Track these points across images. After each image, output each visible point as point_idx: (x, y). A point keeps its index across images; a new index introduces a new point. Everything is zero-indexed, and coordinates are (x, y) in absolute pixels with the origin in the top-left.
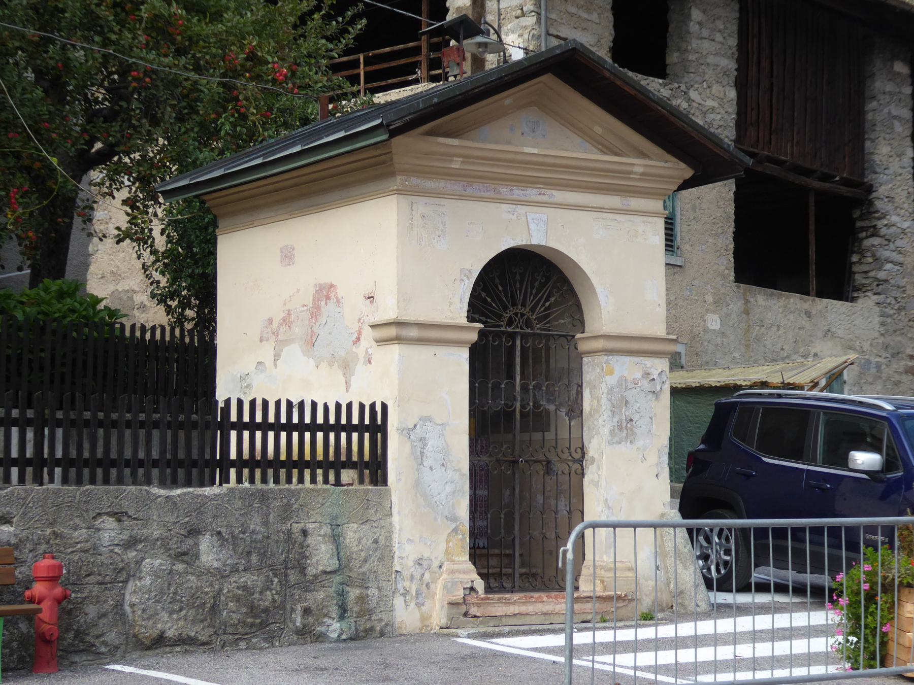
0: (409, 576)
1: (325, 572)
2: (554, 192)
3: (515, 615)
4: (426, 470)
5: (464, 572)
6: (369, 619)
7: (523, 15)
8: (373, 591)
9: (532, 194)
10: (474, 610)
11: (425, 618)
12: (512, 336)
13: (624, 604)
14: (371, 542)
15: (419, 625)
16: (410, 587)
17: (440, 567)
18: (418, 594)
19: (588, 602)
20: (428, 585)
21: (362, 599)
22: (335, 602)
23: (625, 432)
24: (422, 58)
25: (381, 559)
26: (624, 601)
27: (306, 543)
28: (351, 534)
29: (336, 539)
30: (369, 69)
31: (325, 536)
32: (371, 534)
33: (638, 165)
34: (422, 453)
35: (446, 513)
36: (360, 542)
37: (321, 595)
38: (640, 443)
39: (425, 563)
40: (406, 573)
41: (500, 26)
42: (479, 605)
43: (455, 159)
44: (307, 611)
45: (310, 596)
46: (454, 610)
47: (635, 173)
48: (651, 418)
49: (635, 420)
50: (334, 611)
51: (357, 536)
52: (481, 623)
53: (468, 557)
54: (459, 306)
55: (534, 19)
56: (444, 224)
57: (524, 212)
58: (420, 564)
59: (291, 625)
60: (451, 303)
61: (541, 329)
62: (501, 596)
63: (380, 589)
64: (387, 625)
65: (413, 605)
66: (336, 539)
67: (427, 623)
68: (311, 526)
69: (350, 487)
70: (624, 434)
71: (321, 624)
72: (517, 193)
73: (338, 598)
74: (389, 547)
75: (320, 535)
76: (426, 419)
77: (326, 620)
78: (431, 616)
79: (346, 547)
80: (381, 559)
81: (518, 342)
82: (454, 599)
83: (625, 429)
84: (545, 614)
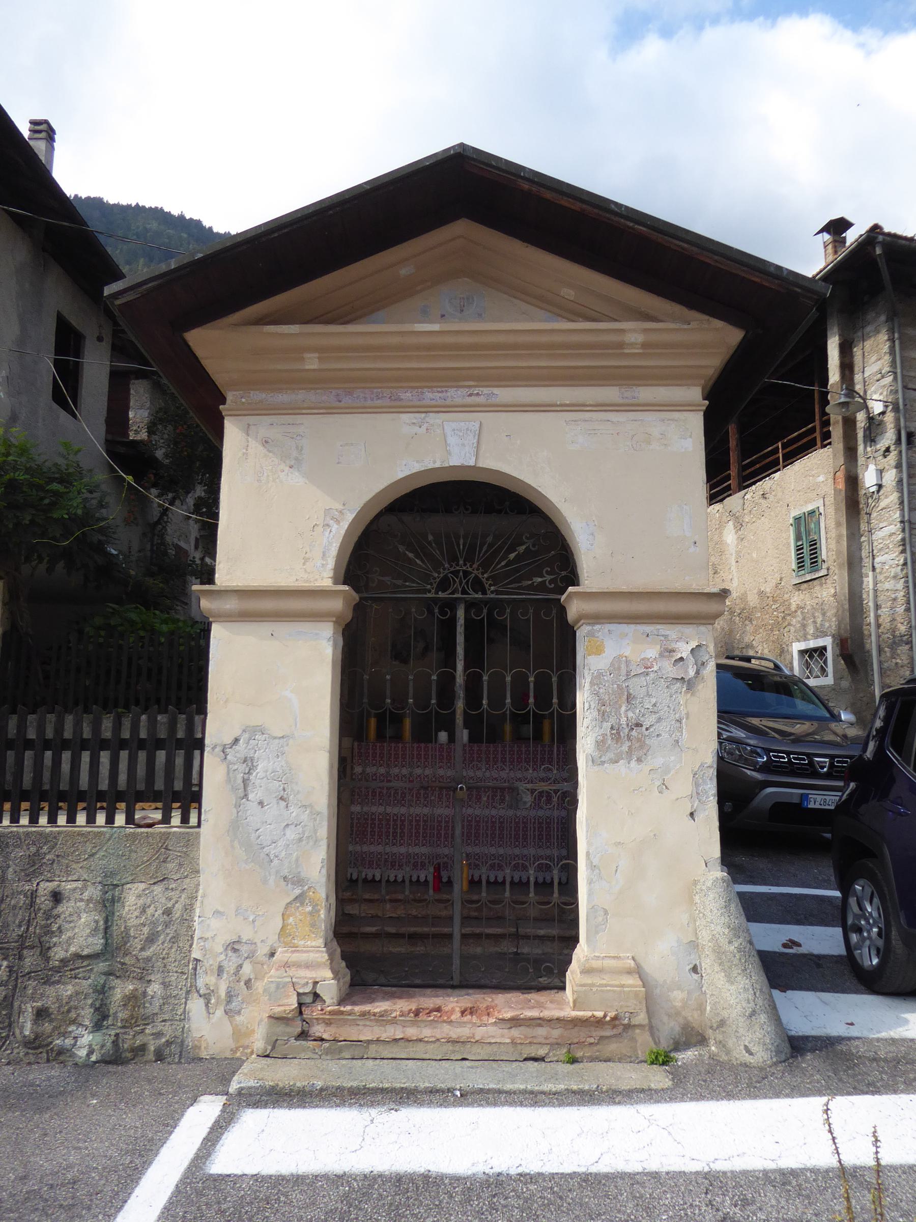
0: (215, 968)
1: (78, 956)
2: (496, 391)
3: (396, 1040)
4: (251, 807)
5: (308, 966)
6: (143, 1031)
7: (883, 377)
8: (155, 988)
9: (456, 395)
10: (318, 1030)
11: (239, 1034)
12: (451, 605)
13: (615, 1031)
14: (160, 912)
15: (230, 1043)
16: (216, 985)
17: (272, 955)
18: (230, 997)
19: (540, 1025)
20: (248, 983)
21: (134, 1000)
22: (90, 1001)
23: (628, 744)
24: (817, 435)
25: (175, 939)
26: (614, 1027)
27: (55, 912)
28: (132, 897)
29: (109, 904)
30: (785, 451)
31: (89, 900)
32: (163, 900)
33: (634, 333)
34: (245, 782)
35: (285, 872)
36: (143, 911)
37: (68, 990)
38: (656, 760)
39: (244, 949)
40: (210, 963)
41: (865, 392)
42: (328, 1023)
43: (307, 355)
44: (41, 1014)
45: (51, 991)
46: (281, 1028)
47: (632, 345)
48: (679, 721)
49: (647, 724)
50: (87, 1015)
51: (141, 902)
52: (328, 1052)
53: (320, 942)
54: (319, 562)
55: (892, 377)
56: (300, 449)
57: (439, 421)
58: (235, 950)
59: (17, 1031)
60: (306, 560)
61: (497, 592)
62: (367, 1008)
63: (166, 985)
64: (168, 1043)
65: (220, 1012)
66: (109, 904)
67: (246, 1042)
68: (70, 886)
69: (149, 830)
70: (625, 748)
71: (65, 1035)
72: (430, 396)
73: (94, 996)
74: (187, 921)
75: (81, 900)
76: (254, 731)
77: (72, 1028)
78: (253, 1031)
79: (120, 917)
80: (175, 939)
81: (461, 614)
82: (278, 1010)
83: (630, 739)
84: (455, 1042)
